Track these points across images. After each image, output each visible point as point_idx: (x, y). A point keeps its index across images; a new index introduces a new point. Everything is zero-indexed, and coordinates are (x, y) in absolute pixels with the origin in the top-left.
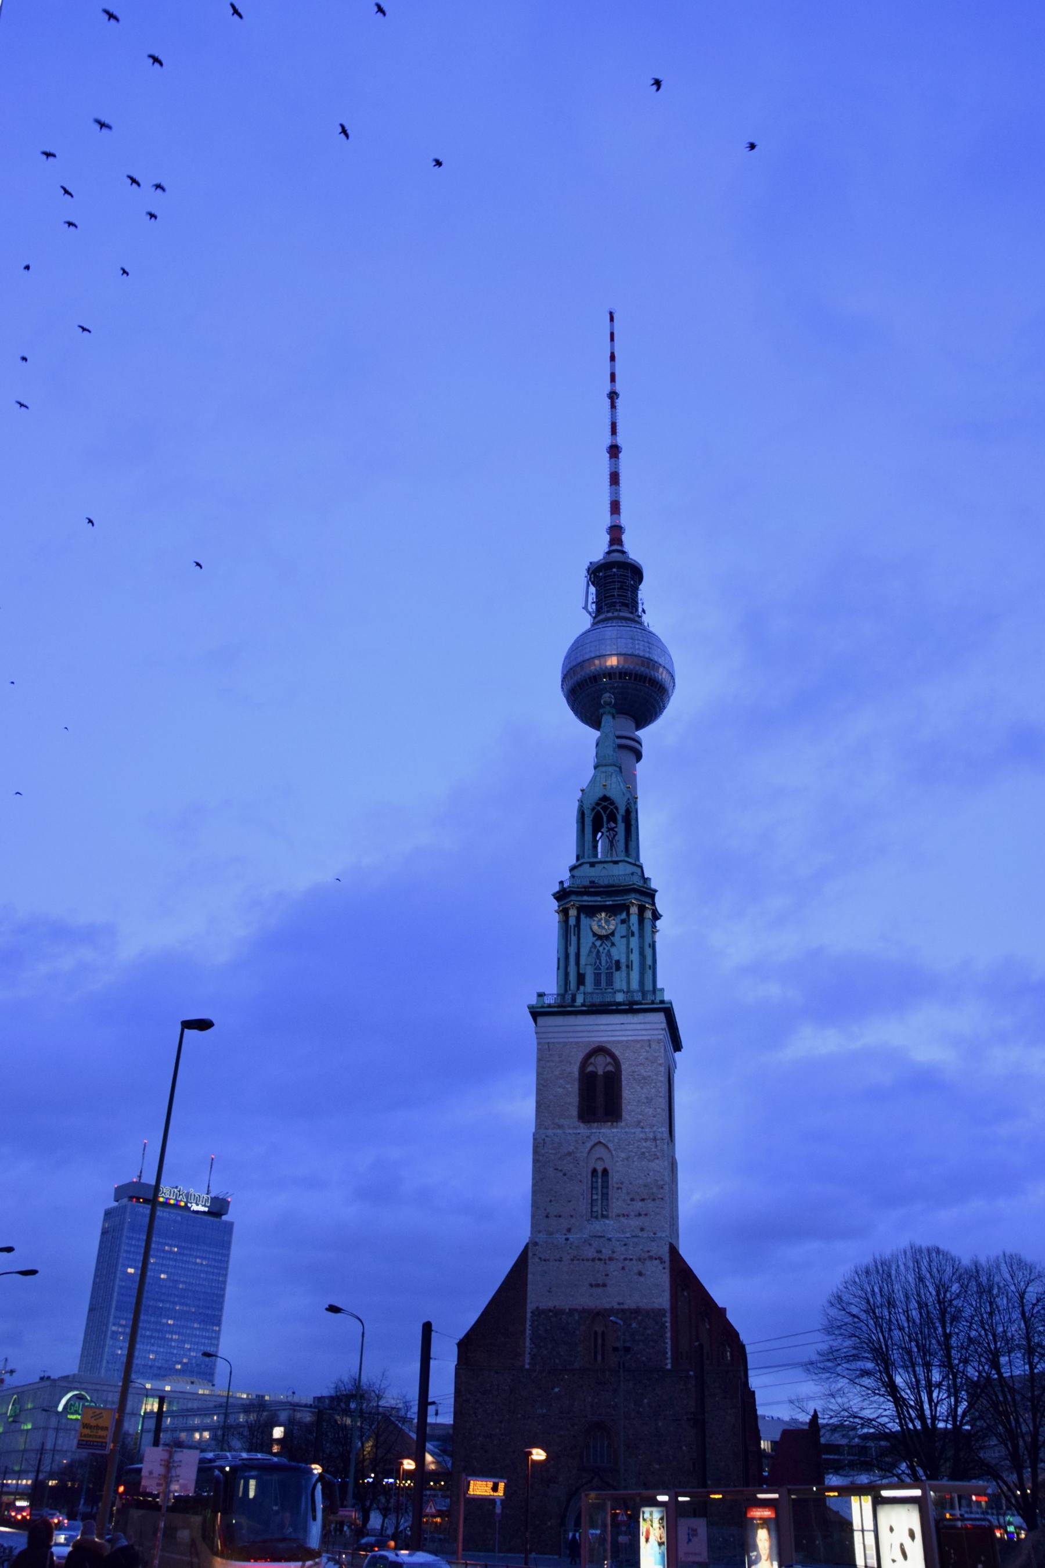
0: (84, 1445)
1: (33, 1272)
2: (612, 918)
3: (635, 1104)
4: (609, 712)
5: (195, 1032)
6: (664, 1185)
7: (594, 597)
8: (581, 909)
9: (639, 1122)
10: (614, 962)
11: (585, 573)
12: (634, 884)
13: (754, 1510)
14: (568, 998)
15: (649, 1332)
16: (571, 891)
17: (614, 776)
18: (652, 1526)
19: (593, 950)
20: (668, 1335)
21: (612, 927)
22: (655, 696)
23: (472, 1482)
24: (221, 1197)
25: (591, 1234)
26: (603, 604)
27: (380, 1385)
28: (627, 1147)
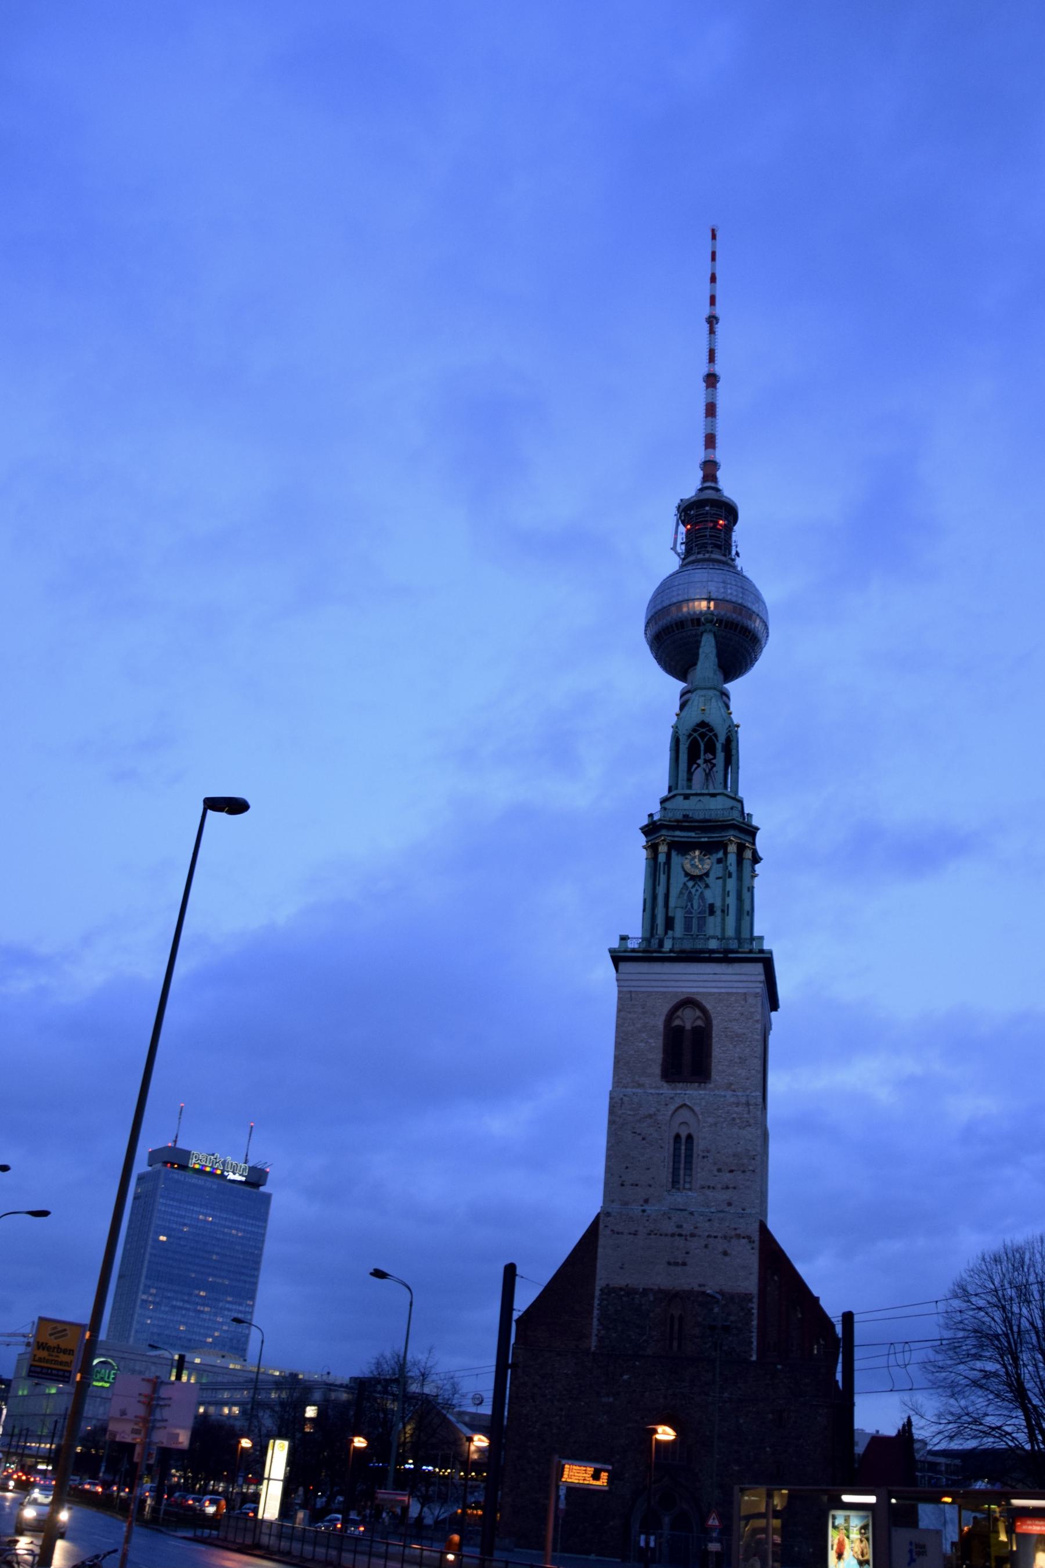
0: (38, 1373)
1: (44, 1213)
3: (726, 1064)
4: (710, 631)
5: (223, 816)
6: (756, 1155)
7: (684, 536)
8: (673, 846)
9: (731, 1084)
10: (707, 906)
11: (674, 511)
12: (733, 819)
13: (1029, 1522)
14: (655, 943)
16: (661, 824)
17: (713, 700)
18: (848, 1537)
19: (684, 891)
20: (755, 1323)
21: (707, 867)
22: (747, 646)
23: (567, 1466)
24: (259, 1167)
25: (672, 1207)
26: (694, 545)
27: (426, 1363)
28: (716, 1112)
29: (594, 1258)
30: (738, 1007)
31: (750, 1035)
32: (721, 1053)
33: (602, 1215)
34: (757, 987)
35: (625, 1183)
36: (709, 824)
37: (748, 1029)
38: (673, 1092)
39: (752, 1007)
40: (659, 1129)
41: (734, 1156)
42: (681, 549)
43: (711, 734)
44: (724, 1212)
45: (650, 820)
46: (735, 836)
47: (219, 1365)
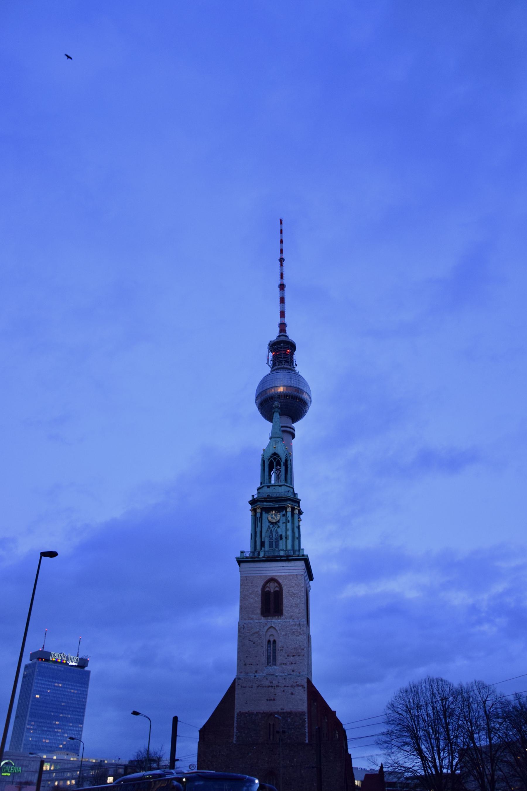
2: (278, 514)
3: (290, 607)
5: (48, 558)
6: (304, 648)
7: (272, 358)
8: (263, 509)
10: (279, 535)
11: (267, 346)
12: (289, 496)
14: (256, 554)
15: (296, 724)
17: (279, 443)
19: (268, 529)
20: (307, 725)
21: (278, 518)
24: (84, 658)
25: (267, 674)
26: (276, 361)
28: (286, 629)
29: (234, 700)
30: (294, 581)
31: (299, 593)
32: (287, 602)
33: (236, 679)
34: (301, 572)
35: (246, 664)
36: (279, 499)
37: (298, 591)
38: (266, 621)
39: (300, 581)
40: (260, 638)
41: (294, 649)
42: (271, 363)
43: (278, 458)
44: (291, 675)
45: (253, 498)
46: (290, 504)
47: (65, 759)
